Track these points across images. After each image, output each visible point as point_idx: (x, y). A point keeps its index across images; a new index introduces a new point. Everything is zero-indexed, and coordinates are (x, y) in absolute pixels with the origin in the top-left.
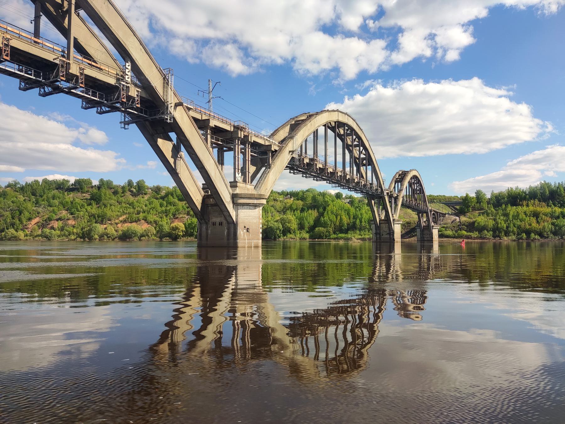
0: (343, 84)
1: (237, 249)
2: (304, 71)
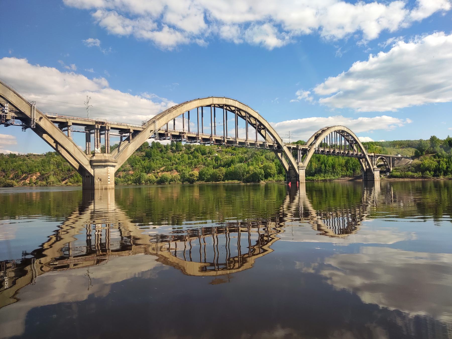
0: (367, 44)
1: (94, 191)
2: (330, 37)
